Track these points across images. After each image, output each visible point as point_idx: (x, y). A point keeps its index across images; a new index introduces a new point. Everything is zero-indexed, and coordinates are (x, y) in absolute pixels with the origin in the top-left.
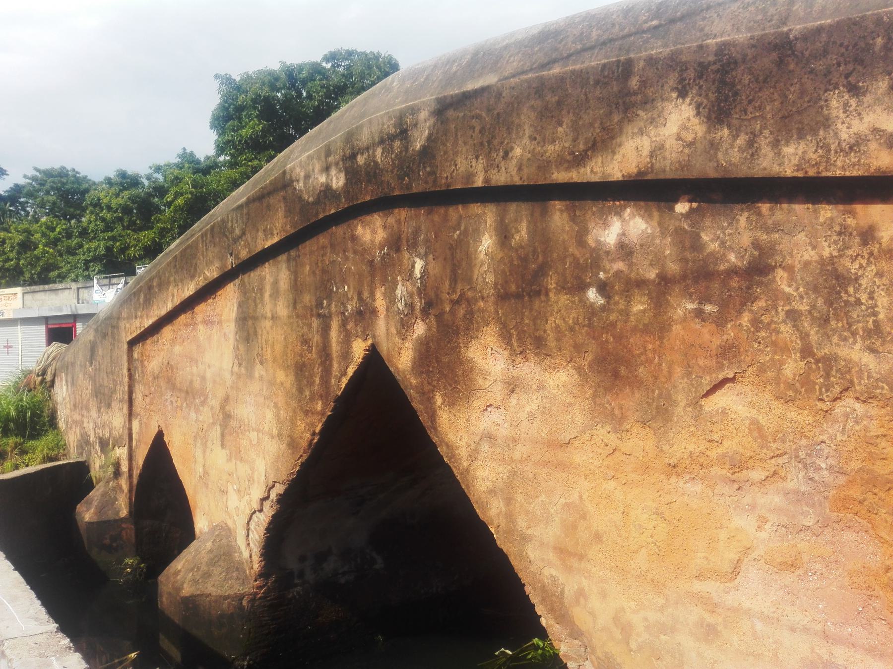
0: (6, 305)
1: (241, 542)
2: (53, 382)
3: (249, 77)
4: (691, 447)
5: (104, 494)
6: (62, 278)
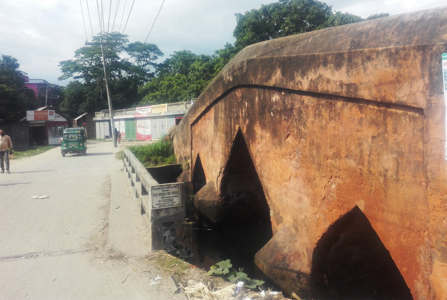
0: (162, 110)
1: (216, 186)
2: (173, 138)
3: (249, 13)
5: (185, 174)
6: (182, 99)
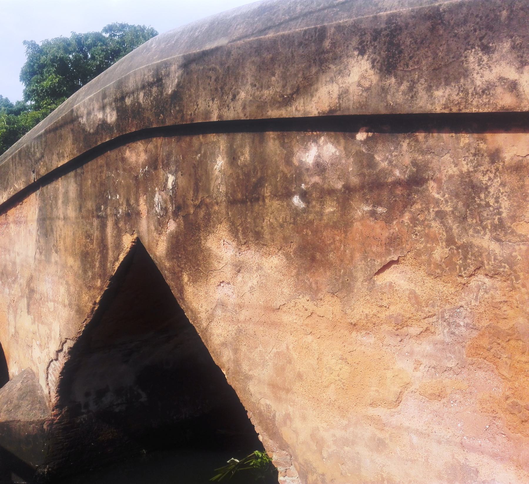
3: (49, 43)
4: (367, 311)
